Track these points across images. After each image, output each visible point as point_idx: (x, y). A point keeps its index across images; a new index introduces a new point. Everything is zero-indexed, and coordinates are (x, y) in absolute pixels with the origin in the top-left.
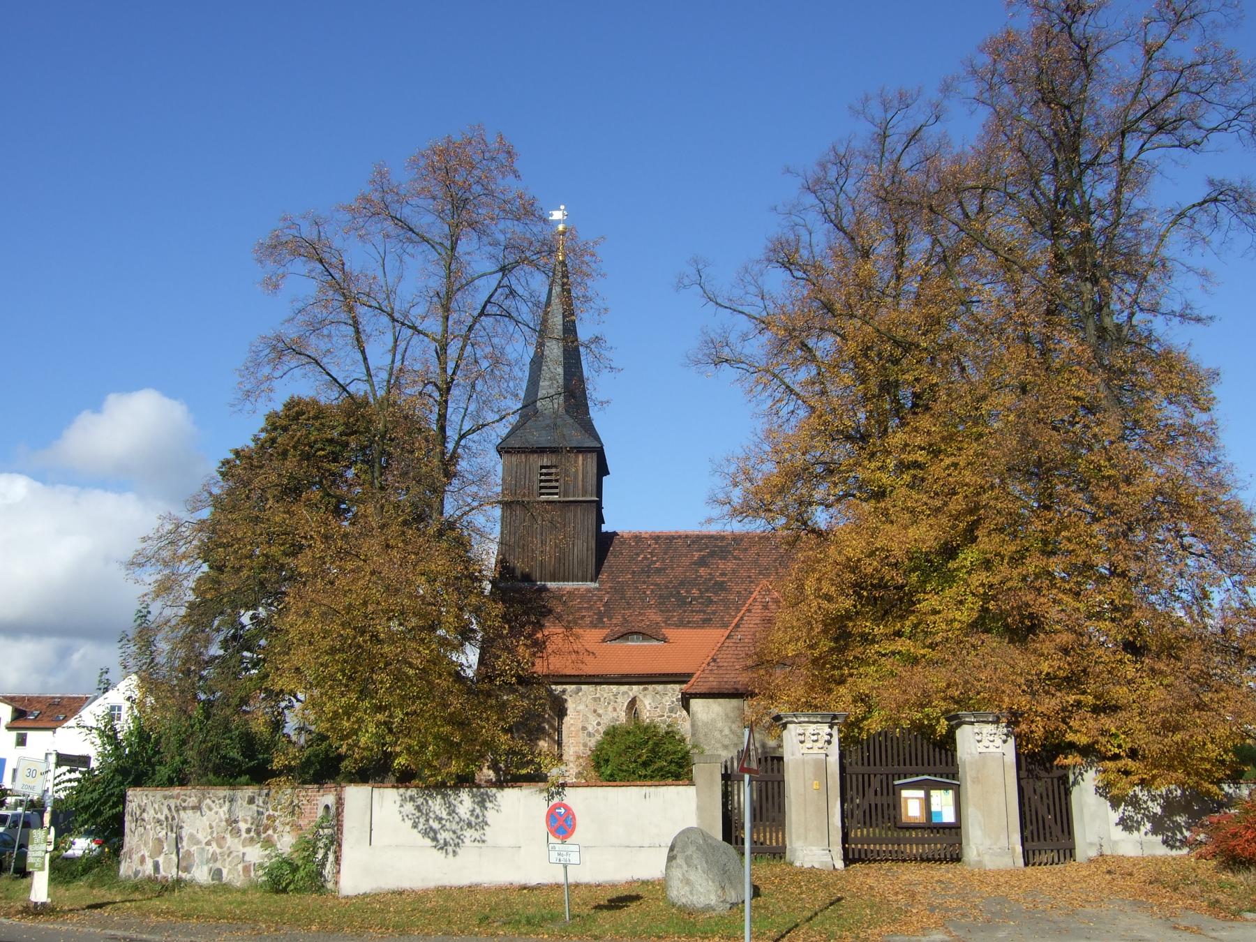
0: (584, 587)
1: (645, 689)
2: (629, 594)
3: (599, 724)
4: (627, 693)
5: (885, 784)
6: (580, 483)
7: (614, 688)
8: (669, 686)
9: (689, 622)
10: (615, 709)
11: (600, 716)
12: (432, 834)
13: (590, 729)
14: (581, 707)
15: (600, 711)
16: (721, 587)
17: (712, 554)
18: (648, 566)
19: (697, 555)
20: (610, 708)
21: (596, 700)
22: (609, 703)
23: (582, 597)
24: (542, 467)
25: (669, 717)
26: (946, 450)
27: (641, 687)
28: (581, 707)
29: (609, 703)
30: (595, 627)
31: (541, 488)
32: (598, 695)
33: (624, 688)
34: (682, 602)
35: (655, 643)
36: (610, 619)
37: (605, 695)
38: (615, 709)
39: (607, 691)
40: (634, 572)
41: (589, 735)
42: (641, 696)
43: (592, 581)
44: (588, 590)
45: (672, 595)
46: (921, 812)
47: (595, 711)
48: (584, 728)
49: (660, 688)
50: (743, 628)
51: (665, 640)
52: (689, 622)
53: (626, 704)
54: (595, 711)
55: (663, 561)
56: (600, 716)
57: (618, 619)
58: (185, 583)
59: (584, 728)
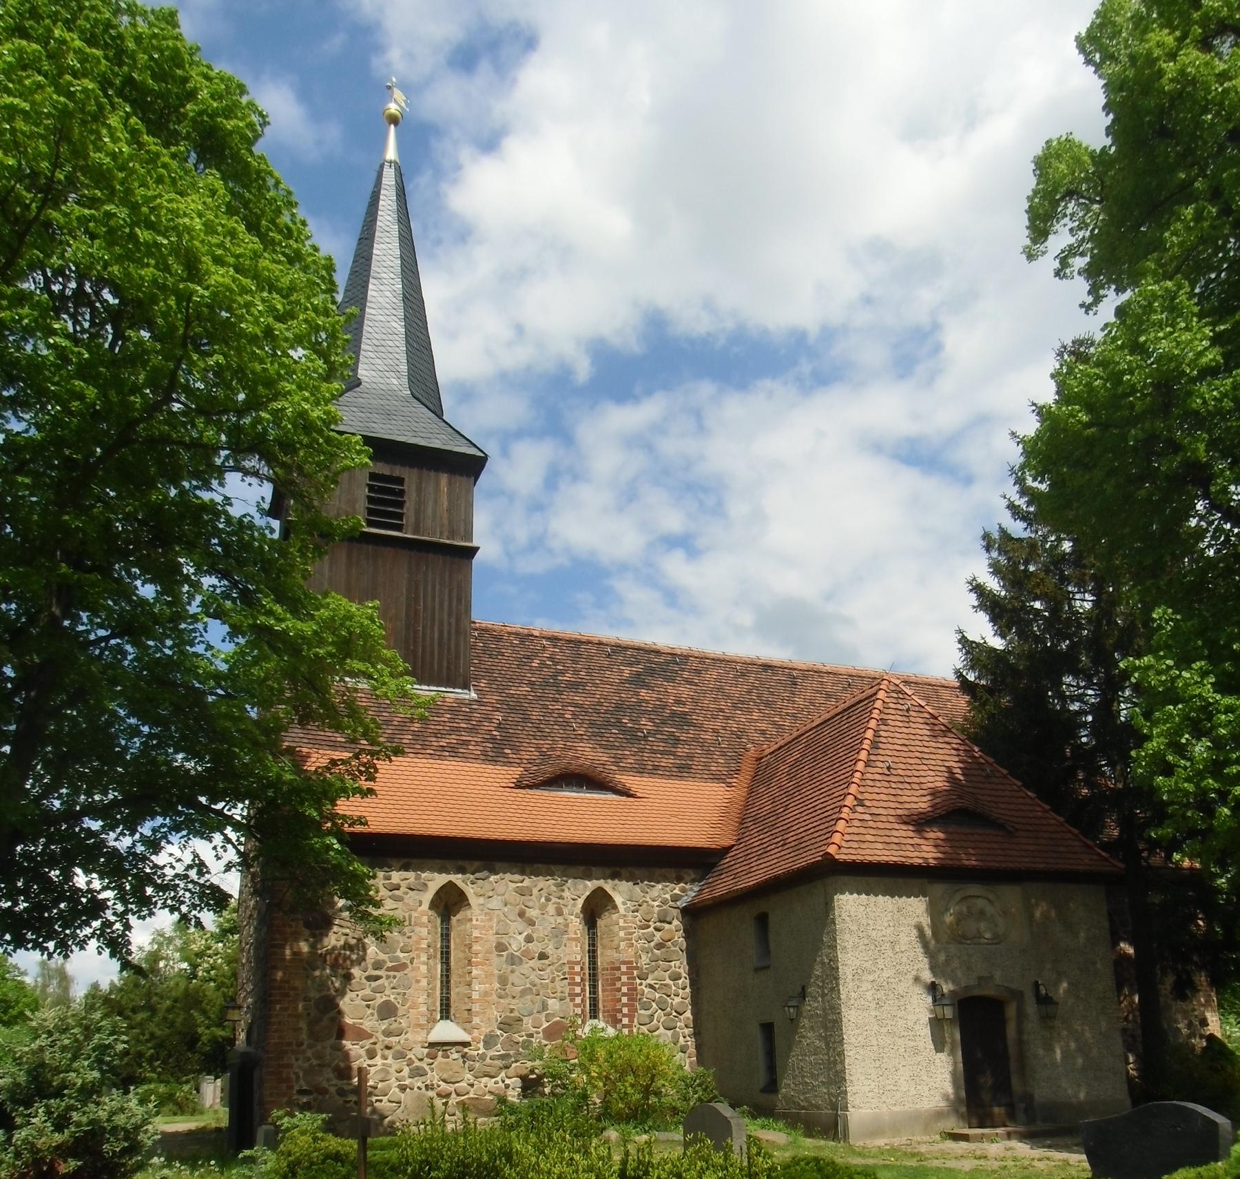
2: (535, 715)
9: (656, 768)
10: (559, 913)
15: (533, 913)
16: (683, 720)
17: (651, 672)
18: (554, 677)
19: (627, 672)
20: (551, 909)
22: (548, 900)
25: (657, 929)
29: (548, 900)
30: (493, 761)
34: (633, 736)
35: (611, 796)
36: (516, 750)
38: (559, 913)
40: (531, 683)
44: (461, 702)
48: (501, 947)
50: (886, 748)
51: (626, 793)
52: (656, 768)
53: (580, 902)
54: (521, 914)
55: (576, 672)
57: (529, 753)
58: (227, 452)
59: (501, 947)
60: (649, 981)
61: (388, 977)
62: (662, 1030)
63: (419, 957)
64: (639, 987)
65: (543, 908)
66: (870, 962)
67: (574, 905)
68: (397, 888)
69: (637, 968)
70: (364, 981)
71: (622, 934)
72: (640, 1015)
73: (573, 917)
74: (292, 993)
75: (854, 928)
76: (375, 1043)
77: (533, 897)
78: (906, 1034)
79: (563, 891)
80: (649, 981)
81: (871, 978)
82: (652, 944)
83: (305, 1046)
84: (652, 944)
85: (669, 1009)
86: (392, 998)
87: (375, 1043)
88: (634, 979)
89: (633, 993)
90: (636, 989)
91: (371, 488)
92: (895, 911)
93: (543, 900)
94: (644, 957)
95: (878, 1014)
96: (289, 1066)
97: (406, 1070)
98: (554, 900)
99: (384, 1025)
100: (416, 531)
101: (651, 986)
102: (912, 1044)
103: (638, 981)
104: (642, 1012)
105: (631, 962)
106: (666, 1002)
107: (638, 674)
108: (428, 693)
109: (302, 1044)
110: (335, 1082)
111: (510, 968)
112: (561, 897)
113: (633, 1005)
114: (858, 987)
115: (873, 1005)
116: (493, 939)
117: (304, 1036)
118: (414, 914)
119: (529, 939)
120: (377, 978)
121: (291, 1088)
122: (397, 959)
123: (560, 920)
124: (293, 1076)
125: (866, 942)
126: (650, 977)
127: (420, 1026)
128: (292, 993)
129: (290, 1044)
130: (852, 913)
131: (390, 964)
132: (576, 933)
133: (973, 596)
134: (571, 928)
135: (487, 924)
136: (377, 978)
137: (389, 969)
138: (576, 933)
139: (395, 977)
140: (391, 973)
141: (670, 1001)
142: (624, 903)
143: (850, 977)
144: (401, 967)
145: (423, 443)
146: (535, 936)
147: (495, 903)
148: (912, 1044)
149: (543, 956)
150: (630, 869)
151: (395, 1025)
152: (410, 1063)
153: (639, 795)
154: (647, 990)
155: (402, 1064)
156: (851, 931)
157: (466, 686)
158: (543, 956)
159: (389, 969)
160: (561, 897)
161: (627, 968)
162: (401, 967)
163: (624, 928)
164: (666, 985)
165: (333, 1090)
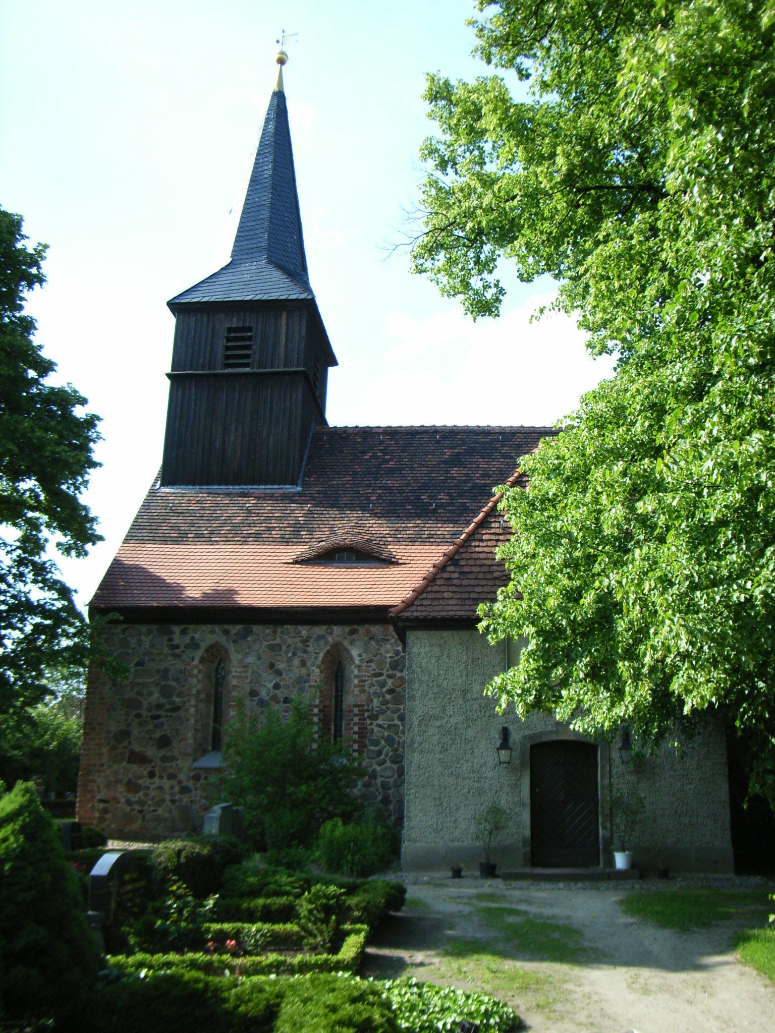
0: (281, 491)
6: (282, 351)
10: (303, 664)
15: (281, 666)
17: (470, 452)
20: (296, 662)
22: (294, 654)
24: (230, 330)
29: (294, 654)
31: (227, 357)
38: (303, 664)
43: (292, 484)
52: (431, 536)
59: (253, 693)
60: (380, 722)
61: (166, 716)
62: (388, 764)
63: (189, 700)
64: (369, 727)
65: (290, 660)
66: (438, 710)
67: (316, 658)
68: (177, 647)
69: (367, 710)
70: (149, 719)
71: (356, 681)
72: (369, 750)
73: (314, 668)
74: (98, 728)
75: (425, 678)
76: (154, 767)
77: (282, 653)
78: (471, 775)
79: (308, 646)
80: (380, 722)
81: (438, 723)
82: (384, 690)
83: (105, 767)
84: (384, 690)
85: (396, 746)
86: (168, 733)
87: (154, 767)
88: (365, 720)
89: (363, 733)
90: (366, 728)
91: (229, 339)
92: (470, 661)
93: (290, 654)
94: (375, 701)
95: (442, 756)
96: (94, 781)
97: (177, 789)
98: (300, 654)
99: (162, 752)
100: (285, 366)
101: (380, 726)
102: (476, 785)
103: (368, 722)
104: (372, 748)
105: (363, 706)
106: (393, 739)
107: (458, 454)
108: (279, 491)
109: (102, 765)
110: (125, 794)
111: (260, 710)
112: (305, 652)
113: (363, 742)
114: (424, 732)
115: (438, 749)
116: (248, 689)
117: (105, 759)
118: (189, 668)
119: (277, 686)
120: (159, 717)
121: (93, 797)
122: (174, 702)
123: (304, 671)
124: (96, 789)
125: (436, 690)
126: (381, 717)
127: (187, 754)
128: (98, 728)
129: (94, 765)
130: (423, 664)
131: (168, 707)
132: (316, 681)
133: (45, 354)
134: (312, 678)
135: (243, 675)
136: (159, 717)
137: (167, 710)
138: (316, 681)
139: (171, 717)
140: (169, 714)
141: (397, 739)
142: (360, 655)
143: (417, 723)
144: (177, 709)
145: (265, 297)
146: (282, 683)
147: (251, 659)
148: (476, 785)
149: (286, 700)
150: (366, 626)
151: (169, 754)
152: (180, 782)
153: (400, 561)
154: (376, 729)
155: (174, 782)
156: (420, 681)
157: (293, 482)
158: (286, 700)
159: (167, 710)
160: (305, 652)
161: (360, 710)
162: (177, 709)
163: (356, 677)
164: (394, 725)
165: (123, 800)
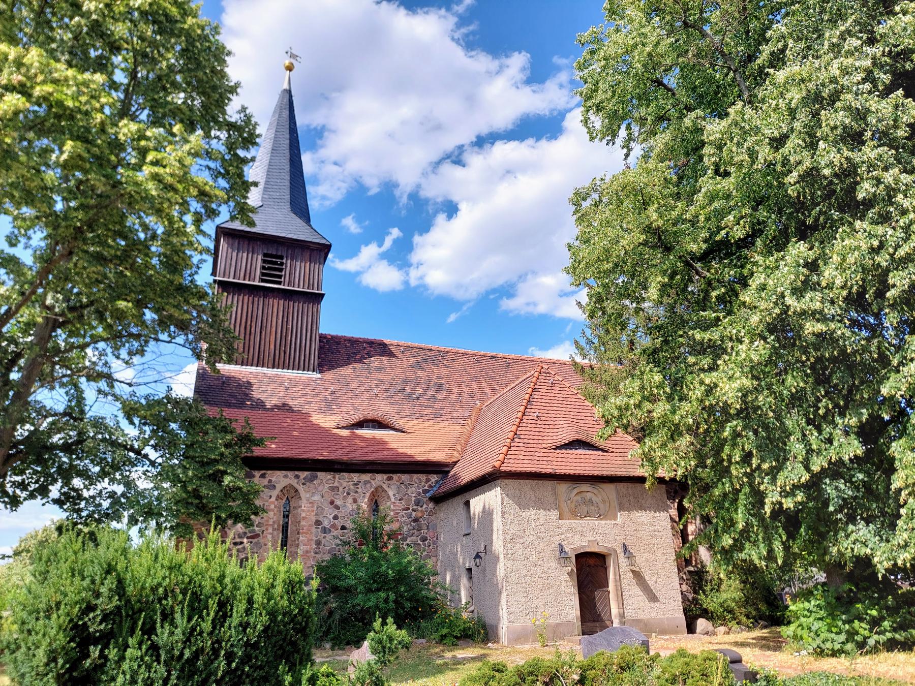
1: (390, 479)
2: (354, 386)
3: (336, 517)
4: (369, 482)
5: (247, 345)
7: (355, 477)
8: (415, 476)
11: (337, 508)
12: (13, 647)
13: (326, 523)
14: (317, 498)
15: (338, 502)
16: (441, 387)
17: (425, 361)
20: (350, 500)
21: (333, 489)
22: (348, 494)
23: (304, 384)
25: (414, 510)
26: (109, 94)
27: (385, 476)
28: (317, 498)
29: (348, 494)
32: (336, 484)
33: (366, 477)
35: (392, 432)
37: (345, 484)
38: (355, 501)
39: (346, 480)
41: (325, 530)
42: (385, 486)
44: (310, 379)
45: (397, 390)
46: (496, 486)
47: (332, 503)
48: (318, 523)
49: (405, 477)
52: (421, 415)
54: (332, 503)
56: (337, 508)
59: (318, 523)
